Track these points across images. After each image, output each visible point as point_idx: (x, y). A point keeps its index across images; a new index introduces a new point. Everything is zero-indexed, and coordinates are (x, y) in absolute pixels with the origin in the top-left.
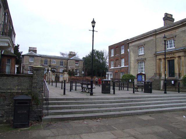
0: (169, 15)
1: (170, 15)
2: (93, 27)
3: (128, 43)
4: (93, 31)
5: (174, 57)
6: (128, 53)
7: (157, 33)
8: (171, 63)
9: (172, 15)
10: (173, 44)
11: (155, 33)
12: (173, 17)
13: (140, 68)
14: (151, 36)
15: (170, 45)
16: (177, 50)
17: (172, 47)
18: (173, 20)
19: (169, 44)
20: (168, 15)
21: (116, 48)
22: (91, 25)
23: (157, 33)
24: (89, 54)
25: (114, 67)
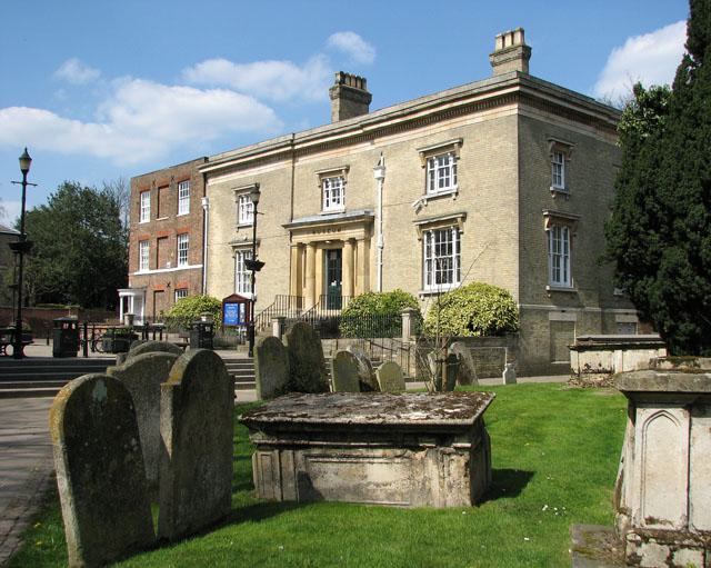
0: (353, 81)
1: (357, 79)
2: (25, 172)
3: (205, 174)
4: (25, 184)
5: (338, 241)
6: (201, 215)
7: (296, 147)
8: (333, 255)
9: (363, 81)
10: (451, 171)
11: (290, 148)
12: (369, 88)
13: (242, 277)
14: (280, 157)
15: (441, 175)
16: (348, 219)
17: (447, 185)
18: (365, 99)
19: (437, 174)
20: (347, 80)
21: (160, 188)
22: (18, 166)
23: (296, 147)
24: (48, 206)
25: (151, 269)
